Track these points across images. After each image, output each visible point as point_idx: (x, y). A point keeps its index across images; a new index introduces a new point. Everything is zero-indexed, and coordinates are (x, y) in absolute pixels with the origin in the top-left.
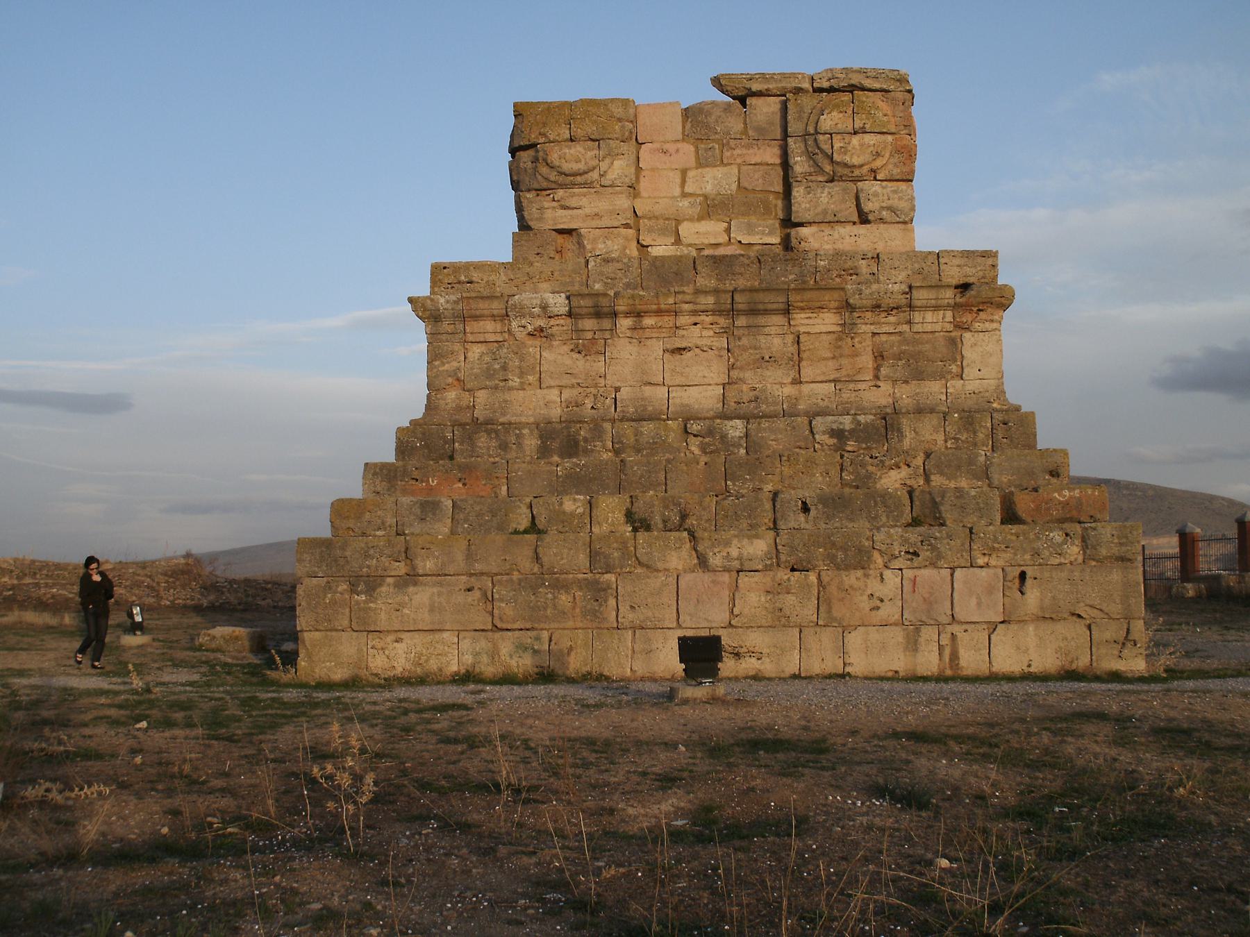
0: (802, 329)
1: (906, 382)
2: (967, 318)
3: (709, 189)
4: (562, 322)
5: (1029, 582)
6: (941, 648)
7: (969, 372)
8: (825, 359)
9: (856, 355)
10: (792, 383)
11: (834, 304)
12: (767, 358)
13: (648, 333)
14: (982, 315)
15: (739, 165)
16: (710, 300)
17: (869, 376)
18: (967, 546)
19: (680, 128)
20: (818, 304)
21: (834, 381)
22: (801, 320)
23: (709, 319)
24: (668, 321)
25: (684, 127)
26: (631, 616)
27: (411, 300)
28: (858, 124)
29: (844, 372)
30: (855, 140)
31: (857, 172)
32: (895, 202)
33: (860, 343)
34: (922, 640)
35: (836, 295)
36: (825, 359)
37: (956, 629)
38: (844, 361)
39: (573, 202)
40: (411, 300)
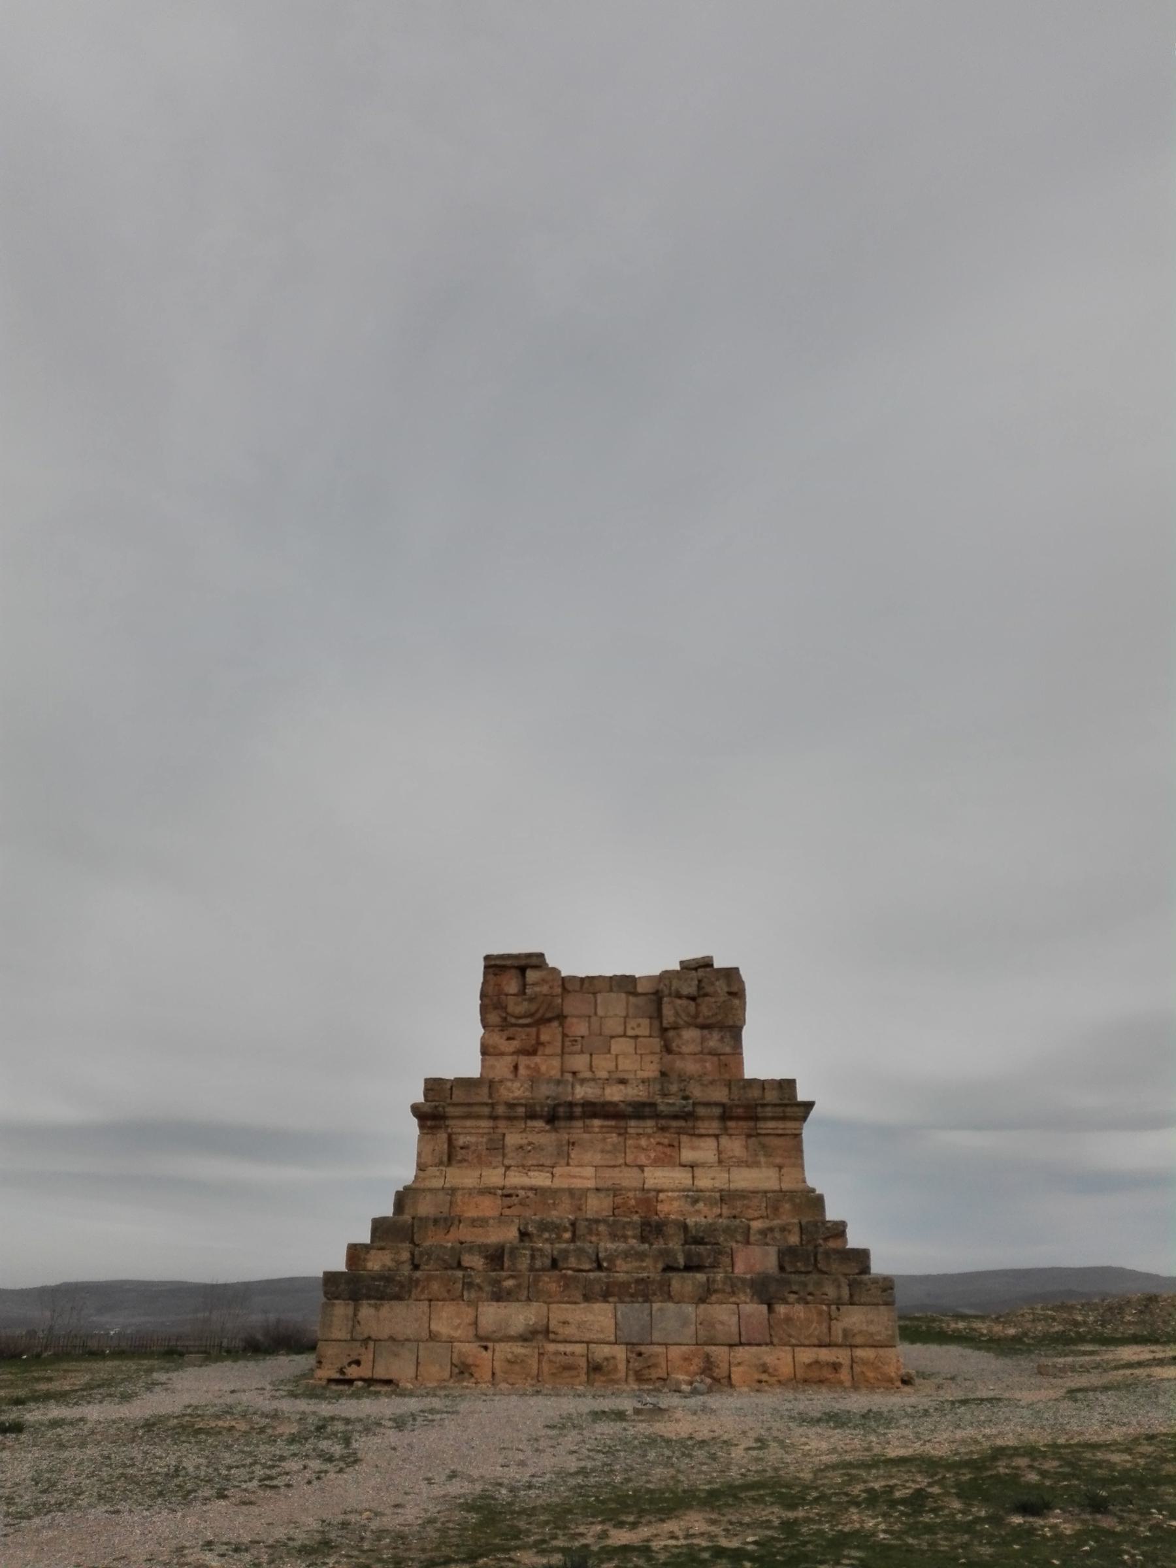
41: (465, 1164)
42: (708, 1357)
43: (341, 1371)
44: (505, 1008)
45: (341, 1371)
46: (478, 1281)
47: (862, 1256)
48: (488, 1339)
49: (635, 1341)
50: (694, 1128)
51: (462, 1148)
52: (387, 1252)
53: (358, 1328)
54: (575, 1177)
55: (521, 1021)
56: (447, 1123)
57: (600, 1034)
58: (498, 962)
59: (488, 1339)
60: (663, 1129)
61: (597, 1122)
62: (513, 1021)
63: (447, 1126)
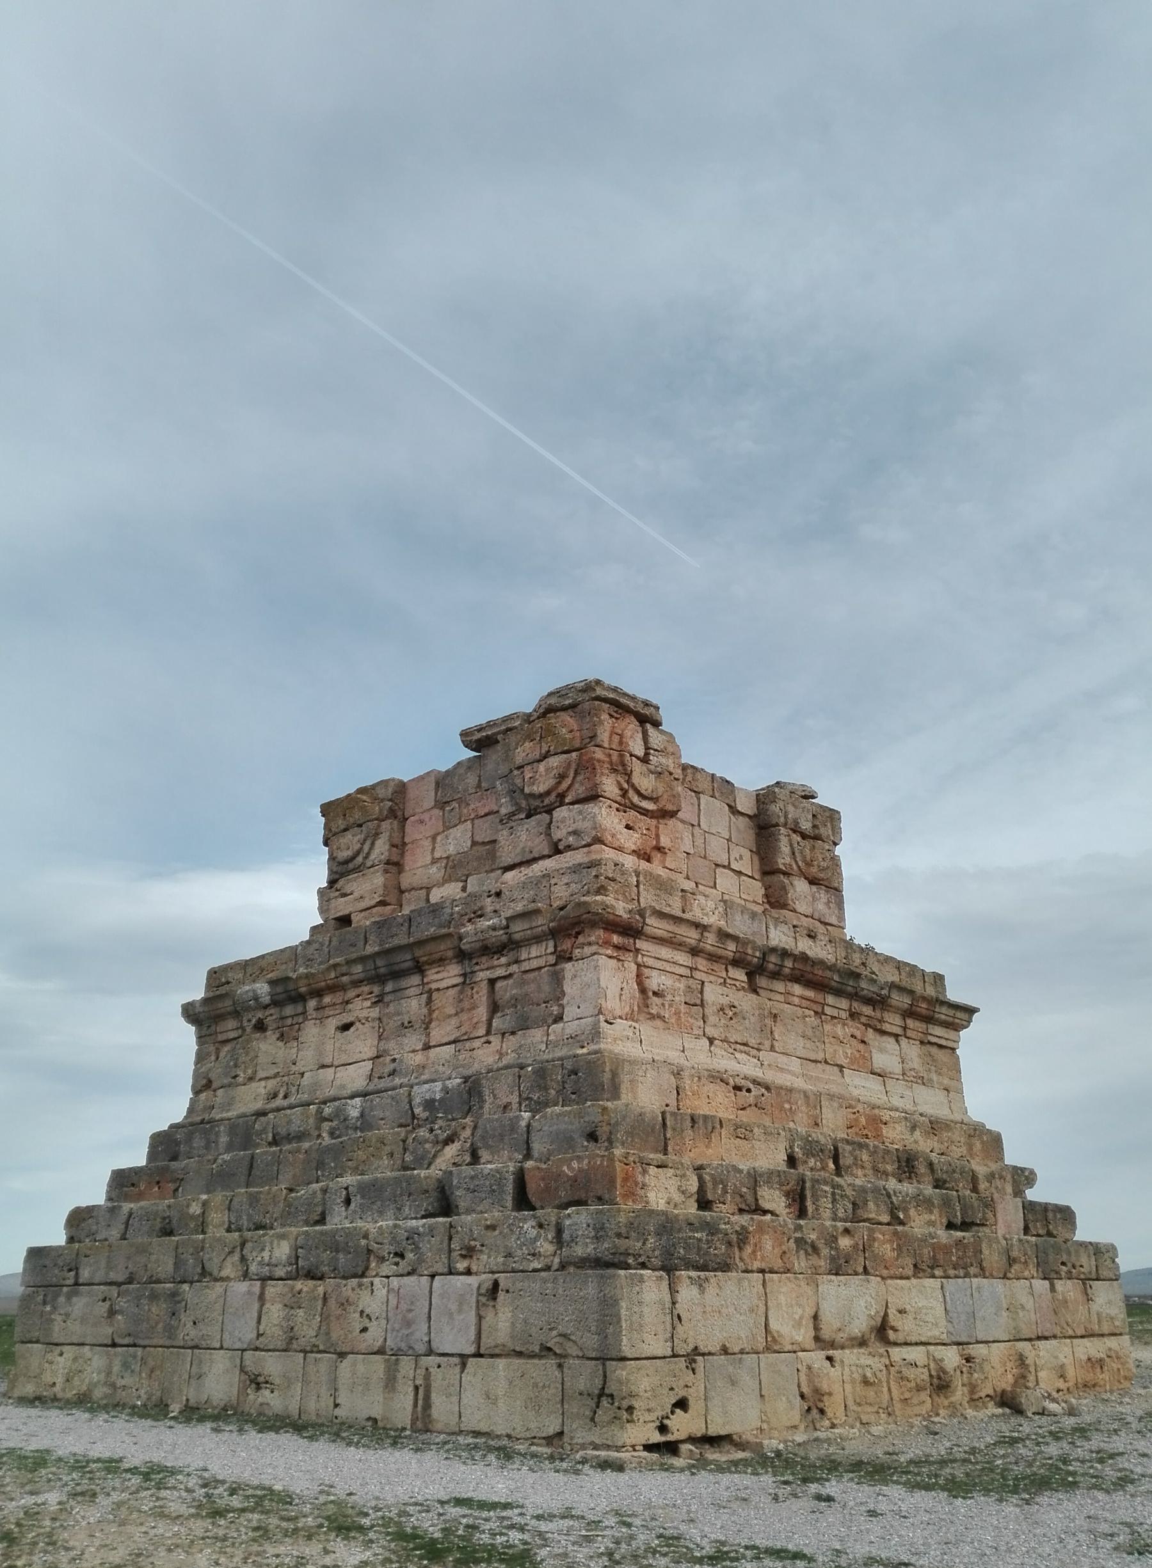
0: (434, 986)
1: (513, 1033)
2: (566, 945)
3: (451, 850)
4: (272, 1011)
5: (501, 1295)
6: (417, 1388)
7: (570, 1012)
8: (450, 1016)
9: (474, 1007)
10: (423, 1050)
11: (450, 954)
12: (406, 1024)
13: (328, 1012)
14: (581, 939)
15: (473, 820)
16: (358, 969)
17: (482, 1031)
18: (445, 1244)
19: (433, 794)
20: (437, 956)
21: (454, 1042)
22: (432, 975)
23: (366, 989)
24: (338, 997)
25: (436, 794)
26: (193, 1333)
27: (971, 1011)
28: (545, 749)
29: (463, 1030)
30: (542, 767)
31: (547, 801)
32: (580, 825)
33: (477, 993)
34: (399, 1376)
35: (449, 943)
36: (450, 1016)
37: (432, 1360)
38: (464, 1016)
39: (348, 890)
40: (971, 1011)
41: (658, 1023)
42: (1021, 1360)
43: (663, 1429)
44: (629, 775)
45: (663, 1429)
46: (813, 1236)
47: (78, 1219)
48: (832, 1345)
49: (964, 1339)
50: (881, 1021)
51: (655, 993)
52: (670, 1172)
53: (679, 1328)
54: (782, 1070)
55: (645, 804)
56: (640, 944)
57: (705, 857)
58: (623, 700)
59: (832, 1345)
60: (853, 1015)
61: (797, 989)
62: (636, 799)
63: (637, 950)
